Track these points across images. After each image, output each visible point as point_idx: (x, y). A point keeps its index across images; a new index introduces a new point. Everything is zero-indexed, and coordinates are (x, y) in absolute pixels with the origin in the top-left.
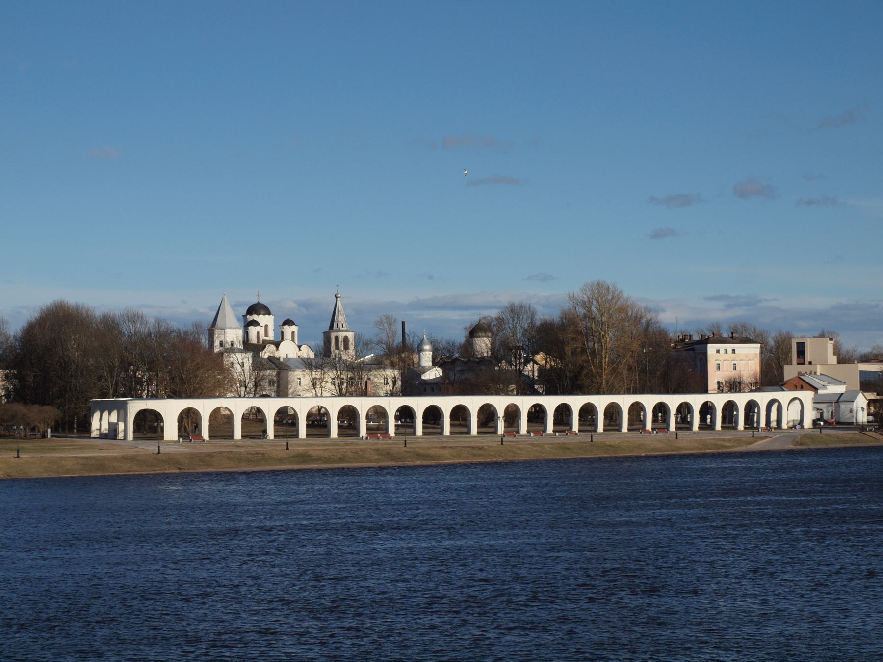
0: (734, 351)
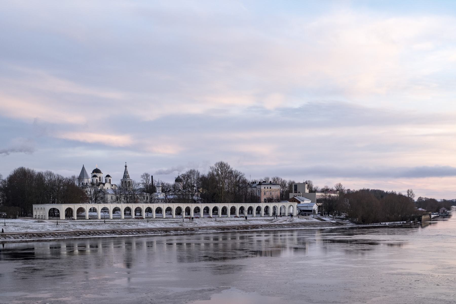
0: (270, 188)
